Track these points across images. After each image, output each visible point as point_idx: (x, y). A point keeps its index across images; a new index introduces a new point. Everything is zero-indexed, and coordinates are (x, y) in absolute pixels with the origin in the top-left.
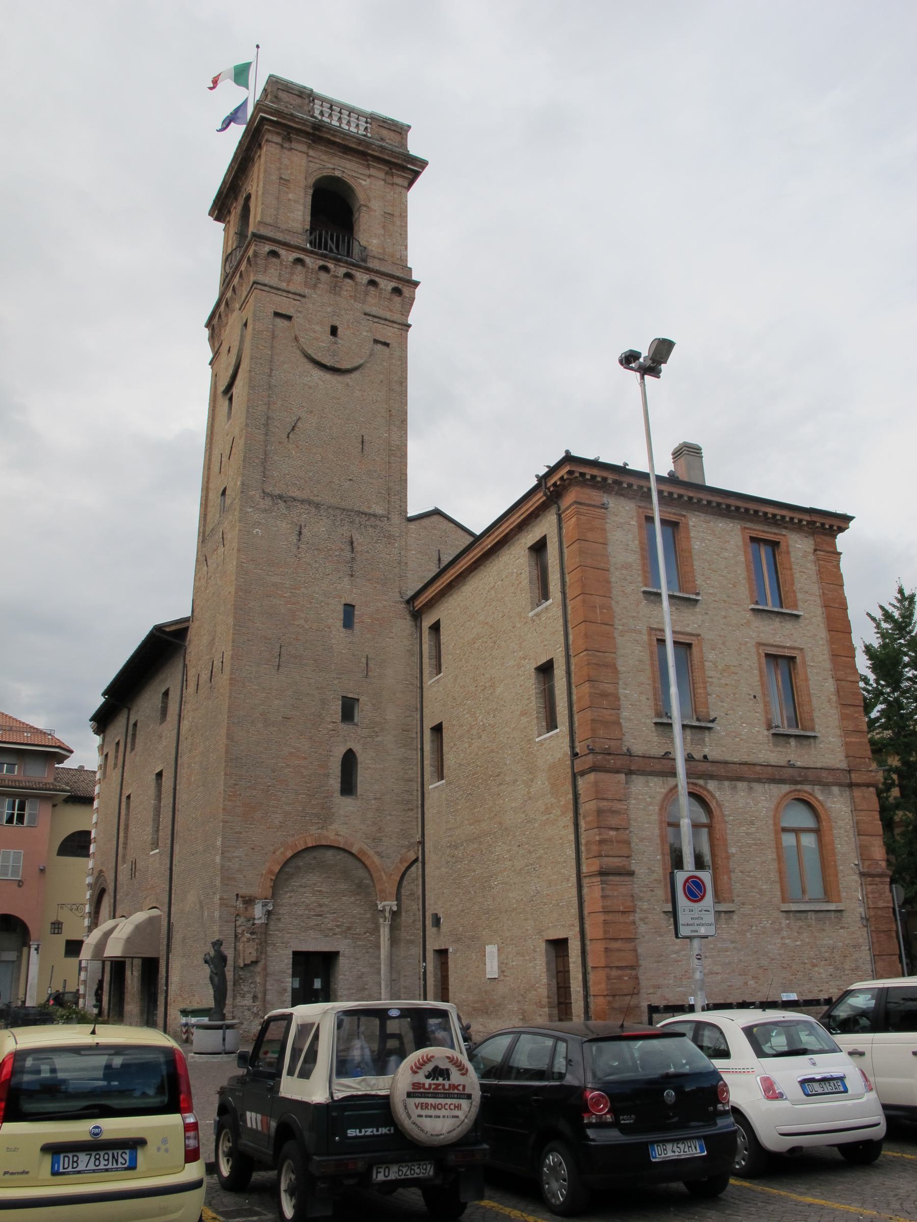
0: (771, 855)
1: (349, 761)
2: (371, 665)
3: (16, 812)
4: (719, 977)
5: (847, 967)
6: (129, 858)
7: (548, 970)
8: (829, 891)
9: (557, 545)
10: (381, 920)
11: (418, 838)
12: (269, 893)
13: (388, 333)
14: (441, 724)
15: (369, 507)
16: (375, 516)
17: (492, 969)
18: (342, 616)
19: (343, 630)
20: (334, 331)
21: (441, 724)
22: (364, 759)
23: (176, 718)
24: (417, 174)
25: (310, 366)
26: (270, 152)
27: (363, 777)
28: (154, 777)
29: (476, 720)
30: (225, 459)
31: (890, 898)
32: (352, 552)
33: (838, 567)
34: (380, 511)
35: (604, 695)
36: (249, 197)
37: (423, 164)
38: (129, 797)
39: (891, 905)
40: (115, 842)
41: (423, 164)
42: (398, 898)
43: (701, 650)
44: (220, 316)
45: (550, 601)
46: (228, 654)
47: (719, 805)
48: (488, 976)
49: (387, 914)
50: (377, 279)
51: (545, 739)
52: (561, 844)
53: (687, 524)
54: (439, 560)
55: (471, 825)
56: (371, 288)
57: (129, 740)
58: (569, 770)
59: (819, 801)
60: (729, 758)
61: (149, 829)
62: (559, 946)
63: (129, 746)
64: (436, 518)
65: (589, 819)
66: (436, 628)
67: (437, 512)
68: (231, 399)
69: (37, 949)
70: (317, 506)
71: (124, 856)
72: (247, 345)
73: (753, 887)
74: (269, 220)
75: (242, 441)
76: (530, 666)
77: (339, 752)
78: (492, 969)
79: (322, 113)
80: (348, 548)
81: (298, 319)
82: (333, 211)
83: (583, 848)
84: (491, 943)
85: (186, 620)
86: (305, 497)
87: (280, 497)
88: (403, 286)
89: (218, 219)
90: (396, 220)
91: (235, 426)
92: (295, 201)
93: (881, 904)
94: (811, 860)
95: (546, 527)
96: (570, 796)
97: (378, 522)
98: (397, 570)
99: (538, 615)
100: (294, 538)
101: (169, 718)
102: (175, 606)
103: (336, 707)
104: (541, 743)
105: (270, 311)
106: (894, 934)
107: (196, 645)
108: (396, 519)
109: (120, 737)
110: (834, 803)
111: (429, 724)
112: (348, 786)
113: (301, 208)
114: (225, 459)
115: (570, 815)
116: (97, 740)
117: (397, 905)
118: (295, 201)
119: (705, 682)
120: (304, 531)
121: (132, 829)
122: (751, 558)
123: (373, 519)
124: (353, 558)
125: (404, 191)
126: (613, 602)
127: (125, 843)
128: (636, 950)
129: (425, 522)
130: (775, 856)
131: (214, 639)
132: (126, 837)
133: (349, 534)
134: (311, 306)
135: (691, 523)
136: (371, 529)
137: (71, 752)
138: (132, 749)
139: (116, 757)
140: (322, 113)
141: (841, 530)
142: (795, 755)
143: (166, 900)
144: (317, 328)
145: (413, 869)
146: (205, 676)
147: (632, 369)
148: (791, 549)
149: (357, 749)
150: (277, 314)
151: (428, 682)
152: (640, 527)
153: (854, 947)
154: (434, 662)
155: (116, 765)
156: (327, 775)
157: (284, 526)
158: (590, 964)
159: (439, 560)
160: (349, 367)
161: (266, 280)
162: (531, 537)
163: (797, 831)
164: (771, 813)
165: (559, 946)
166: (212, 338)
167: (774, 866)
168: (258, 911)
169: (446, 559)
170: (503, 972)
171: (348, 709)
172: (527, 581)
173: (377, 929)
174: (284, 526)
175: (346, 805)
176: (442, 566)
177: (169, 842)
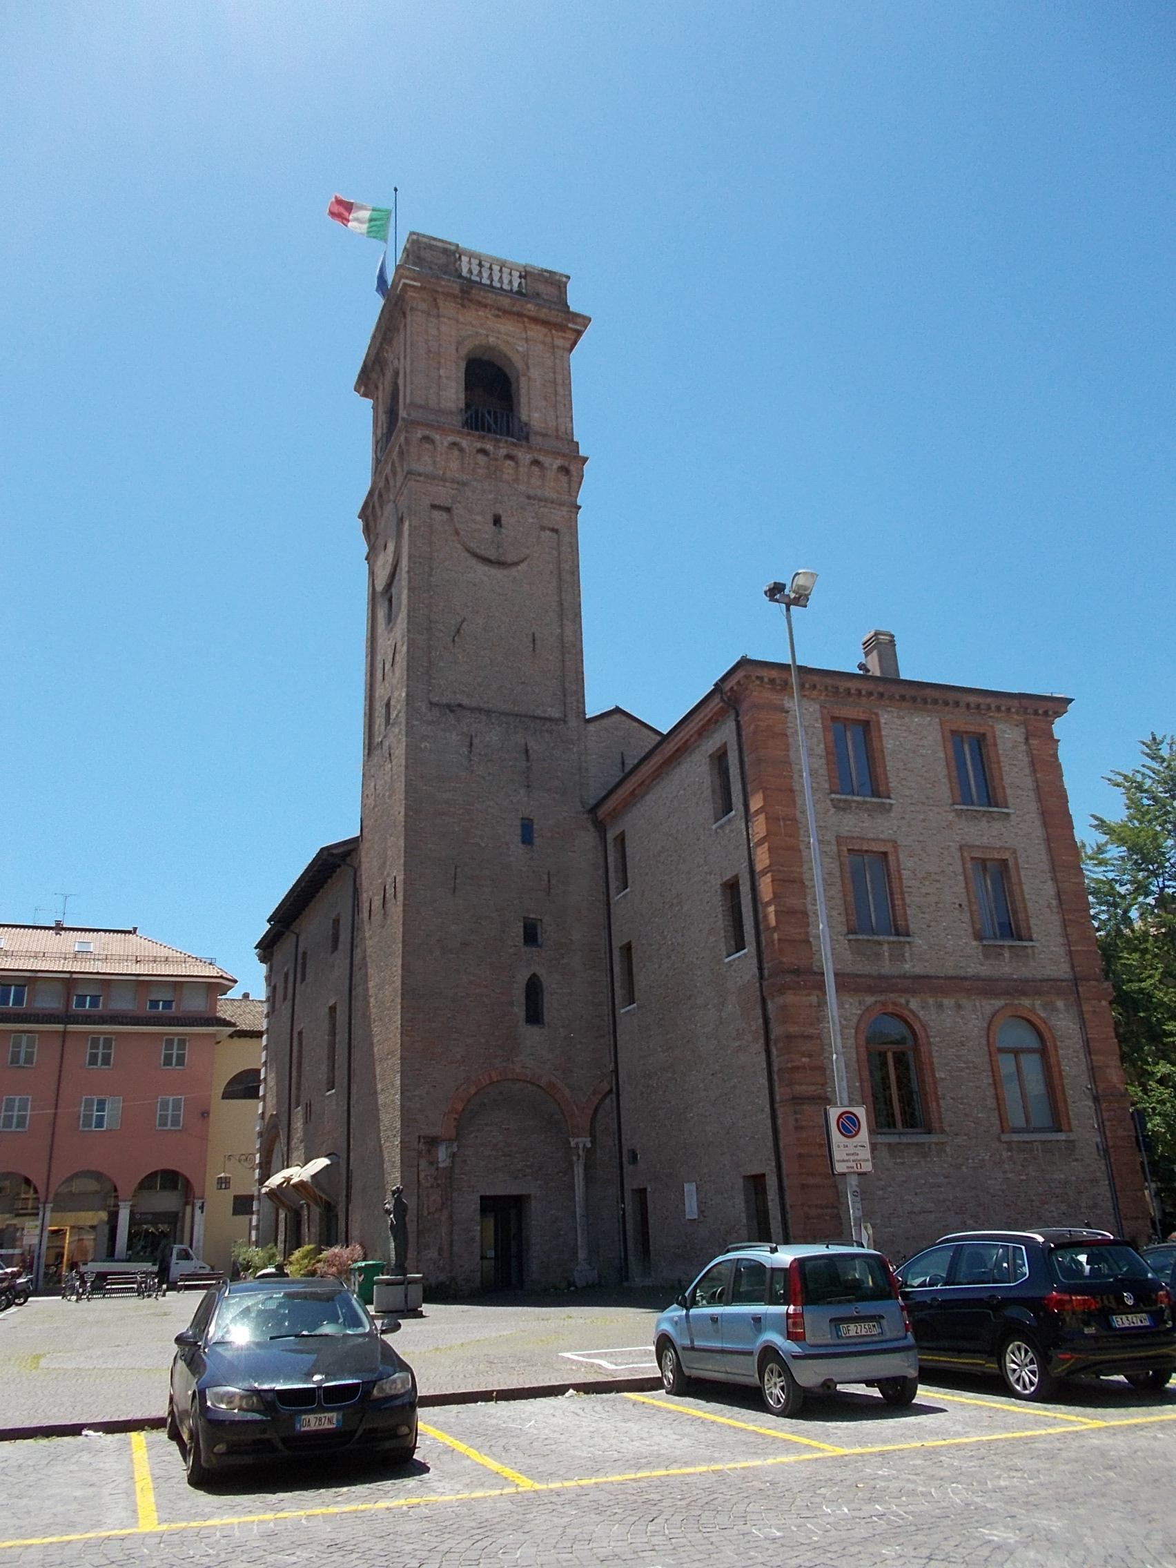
0: (986, 1080)
1: (534, 989)
2: (553, 881)
3: (175, 1052)
4: (932, 1217)
5: (1083, 1205)
6: (304, 1100)
7: (748, 1209)
8: (1058, 1122)
9: (736, 754)
10: (575, 1158)
11: (612, 1067)
12: (453, 1133)
13: (557, 516)
14: (630, 943)
15: (545, 712)
16: (550, 719)
17: (691, 1208)
18: (519, 832)
19: (521, 845)
20: (497, 521)
21: (630, 943)
22: (550, 983)
23: (349, 946)
24: (579, 333)
25: (473, 561)
26: (416, 324)
27: (550, 1004)
28: (327, 1010)
29: (665, 938)
30: (388, 666)
31: (1132, 1126)
32: (528, 760)
33: (1055, 756)
34: (555, 713)
35: (792, 912)
36: (397, 373)
37: (586, 320)
38: (300, 1033)
39: (1133, 1133)
40: (287, 1083)
41: (586, 320)
42: (593, 1136)
43: (898, 859)
44: (373, 507)
45: (733, 813)
46: (400, 878)
47: (924, 1027)
48: (688, 1217)
49: (581, 1152)
50: (541, 458)
51: (734, 960)
52: (755, 1072)
53: (878, 722)
54: (623, 763)
55: (663, 1052)
56: (535, 469)
57: (299, 969)
58: (758, 993)
59: (1040, 1018)
60: (932, 972)
61: (324, 1068)
62: (756, 1183)
63: (299, 975)
64: (617, 717)
65: (781, 1045)
66: (621, 839)
67: (617, 710)
68: (390, 601)
69: (202, 1208)
70: (488, 712)
71: (298, 1097)
72: (404, 563)
73: (966, 1115)
74: (419, 401)
75: (405, 648)
76: (716, 882)
77: (523, 977)
78: (691, 1208)
79: (470, 271)
80: (524, 757)
81: (459, 510)
82: (492, 396)
83: (775, 1077)
84: (689, 1181)
85: (355, 840)
86: (474, 705)
87: (448, 706)
88: (571, 464)
89: (365, 395)
90: (559, 389)
91: (396, 637)
92: (448, 378)
93: (1121, 1133)
94: (1036, 1087)
95: (726, 734)
96: (761, 1021)
97: (554, 727)
98: (577, 777)
99: (721, 827)
100: (465, 750)
101: (341, 946)
102: (345, 828)
103: (518, 929)
104: (730, 964)
105: (427, 502)
106: (1139, 1167)
107: (368, 862)
108: (573, 722)
109: (289, 967)
110: (1059, 1019)
111: (617, 943)
112: (534, 1015)
113: (454, 384)
114: (388, 666)
115: (762, 1041)
116: (263, 968)
117: (592, 1142)
118: (448, 378)
119: (902, 893)
120: (476, 741)
121: (306, 1067)
122: (951, 754)
123: (548, 724)
124: (528, 768)
125: (566, 354)
126: (798, 813)
127: (299, 1083)
128: (836, 1187)
129: (605, 721)
130: (991, 1081)
131: (385, 863)
132: (299, 1076)
133: (523, 742)
134: (470, 494)
135: (883, 721)
136: (546, 735)
137: (236, 981)
138: (303, 979)
139: (286, 988)
140: (470, 271)
141: (1058, 714)
142: (1006, 967)
143: (345, 1145)
144: (479, 518)
145: (607, 1101)
146: (377, 903)
147: (777, 601)
148: (998, 741)
149: (542, 972)
150: (434, 507)
151: (616, 898)
152: (825, 728)
153: (1092, 1181)
154: (620, 875)
155: (285, 999)
156: (511, 1004)
157: (454, 737)
158: (788, 1202)
159: (623, 763)
160: (515, 560)
161: (421, 469)
162: (711, 745)
163: (1016, 1052)
164: (983, 1033)
165: (756, 1183)
166: (367, 530)
167: (990, 1092)
168: (442, 1154)
169: (630, 763)
170: (702, 1212)
171: (531, 935)
172: (709, 791)
173: (571, 1166)
174: (454, 737)
175: (531, 1036)
176: (627, 770)
177: (346, 1080)
